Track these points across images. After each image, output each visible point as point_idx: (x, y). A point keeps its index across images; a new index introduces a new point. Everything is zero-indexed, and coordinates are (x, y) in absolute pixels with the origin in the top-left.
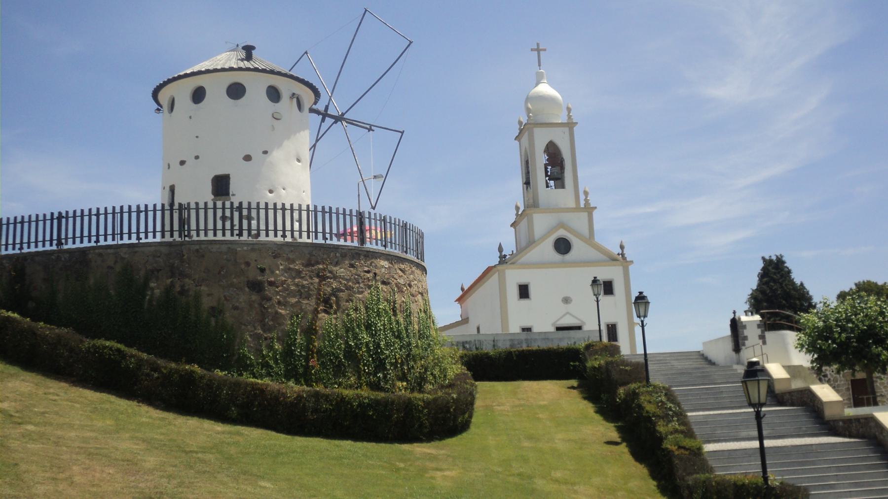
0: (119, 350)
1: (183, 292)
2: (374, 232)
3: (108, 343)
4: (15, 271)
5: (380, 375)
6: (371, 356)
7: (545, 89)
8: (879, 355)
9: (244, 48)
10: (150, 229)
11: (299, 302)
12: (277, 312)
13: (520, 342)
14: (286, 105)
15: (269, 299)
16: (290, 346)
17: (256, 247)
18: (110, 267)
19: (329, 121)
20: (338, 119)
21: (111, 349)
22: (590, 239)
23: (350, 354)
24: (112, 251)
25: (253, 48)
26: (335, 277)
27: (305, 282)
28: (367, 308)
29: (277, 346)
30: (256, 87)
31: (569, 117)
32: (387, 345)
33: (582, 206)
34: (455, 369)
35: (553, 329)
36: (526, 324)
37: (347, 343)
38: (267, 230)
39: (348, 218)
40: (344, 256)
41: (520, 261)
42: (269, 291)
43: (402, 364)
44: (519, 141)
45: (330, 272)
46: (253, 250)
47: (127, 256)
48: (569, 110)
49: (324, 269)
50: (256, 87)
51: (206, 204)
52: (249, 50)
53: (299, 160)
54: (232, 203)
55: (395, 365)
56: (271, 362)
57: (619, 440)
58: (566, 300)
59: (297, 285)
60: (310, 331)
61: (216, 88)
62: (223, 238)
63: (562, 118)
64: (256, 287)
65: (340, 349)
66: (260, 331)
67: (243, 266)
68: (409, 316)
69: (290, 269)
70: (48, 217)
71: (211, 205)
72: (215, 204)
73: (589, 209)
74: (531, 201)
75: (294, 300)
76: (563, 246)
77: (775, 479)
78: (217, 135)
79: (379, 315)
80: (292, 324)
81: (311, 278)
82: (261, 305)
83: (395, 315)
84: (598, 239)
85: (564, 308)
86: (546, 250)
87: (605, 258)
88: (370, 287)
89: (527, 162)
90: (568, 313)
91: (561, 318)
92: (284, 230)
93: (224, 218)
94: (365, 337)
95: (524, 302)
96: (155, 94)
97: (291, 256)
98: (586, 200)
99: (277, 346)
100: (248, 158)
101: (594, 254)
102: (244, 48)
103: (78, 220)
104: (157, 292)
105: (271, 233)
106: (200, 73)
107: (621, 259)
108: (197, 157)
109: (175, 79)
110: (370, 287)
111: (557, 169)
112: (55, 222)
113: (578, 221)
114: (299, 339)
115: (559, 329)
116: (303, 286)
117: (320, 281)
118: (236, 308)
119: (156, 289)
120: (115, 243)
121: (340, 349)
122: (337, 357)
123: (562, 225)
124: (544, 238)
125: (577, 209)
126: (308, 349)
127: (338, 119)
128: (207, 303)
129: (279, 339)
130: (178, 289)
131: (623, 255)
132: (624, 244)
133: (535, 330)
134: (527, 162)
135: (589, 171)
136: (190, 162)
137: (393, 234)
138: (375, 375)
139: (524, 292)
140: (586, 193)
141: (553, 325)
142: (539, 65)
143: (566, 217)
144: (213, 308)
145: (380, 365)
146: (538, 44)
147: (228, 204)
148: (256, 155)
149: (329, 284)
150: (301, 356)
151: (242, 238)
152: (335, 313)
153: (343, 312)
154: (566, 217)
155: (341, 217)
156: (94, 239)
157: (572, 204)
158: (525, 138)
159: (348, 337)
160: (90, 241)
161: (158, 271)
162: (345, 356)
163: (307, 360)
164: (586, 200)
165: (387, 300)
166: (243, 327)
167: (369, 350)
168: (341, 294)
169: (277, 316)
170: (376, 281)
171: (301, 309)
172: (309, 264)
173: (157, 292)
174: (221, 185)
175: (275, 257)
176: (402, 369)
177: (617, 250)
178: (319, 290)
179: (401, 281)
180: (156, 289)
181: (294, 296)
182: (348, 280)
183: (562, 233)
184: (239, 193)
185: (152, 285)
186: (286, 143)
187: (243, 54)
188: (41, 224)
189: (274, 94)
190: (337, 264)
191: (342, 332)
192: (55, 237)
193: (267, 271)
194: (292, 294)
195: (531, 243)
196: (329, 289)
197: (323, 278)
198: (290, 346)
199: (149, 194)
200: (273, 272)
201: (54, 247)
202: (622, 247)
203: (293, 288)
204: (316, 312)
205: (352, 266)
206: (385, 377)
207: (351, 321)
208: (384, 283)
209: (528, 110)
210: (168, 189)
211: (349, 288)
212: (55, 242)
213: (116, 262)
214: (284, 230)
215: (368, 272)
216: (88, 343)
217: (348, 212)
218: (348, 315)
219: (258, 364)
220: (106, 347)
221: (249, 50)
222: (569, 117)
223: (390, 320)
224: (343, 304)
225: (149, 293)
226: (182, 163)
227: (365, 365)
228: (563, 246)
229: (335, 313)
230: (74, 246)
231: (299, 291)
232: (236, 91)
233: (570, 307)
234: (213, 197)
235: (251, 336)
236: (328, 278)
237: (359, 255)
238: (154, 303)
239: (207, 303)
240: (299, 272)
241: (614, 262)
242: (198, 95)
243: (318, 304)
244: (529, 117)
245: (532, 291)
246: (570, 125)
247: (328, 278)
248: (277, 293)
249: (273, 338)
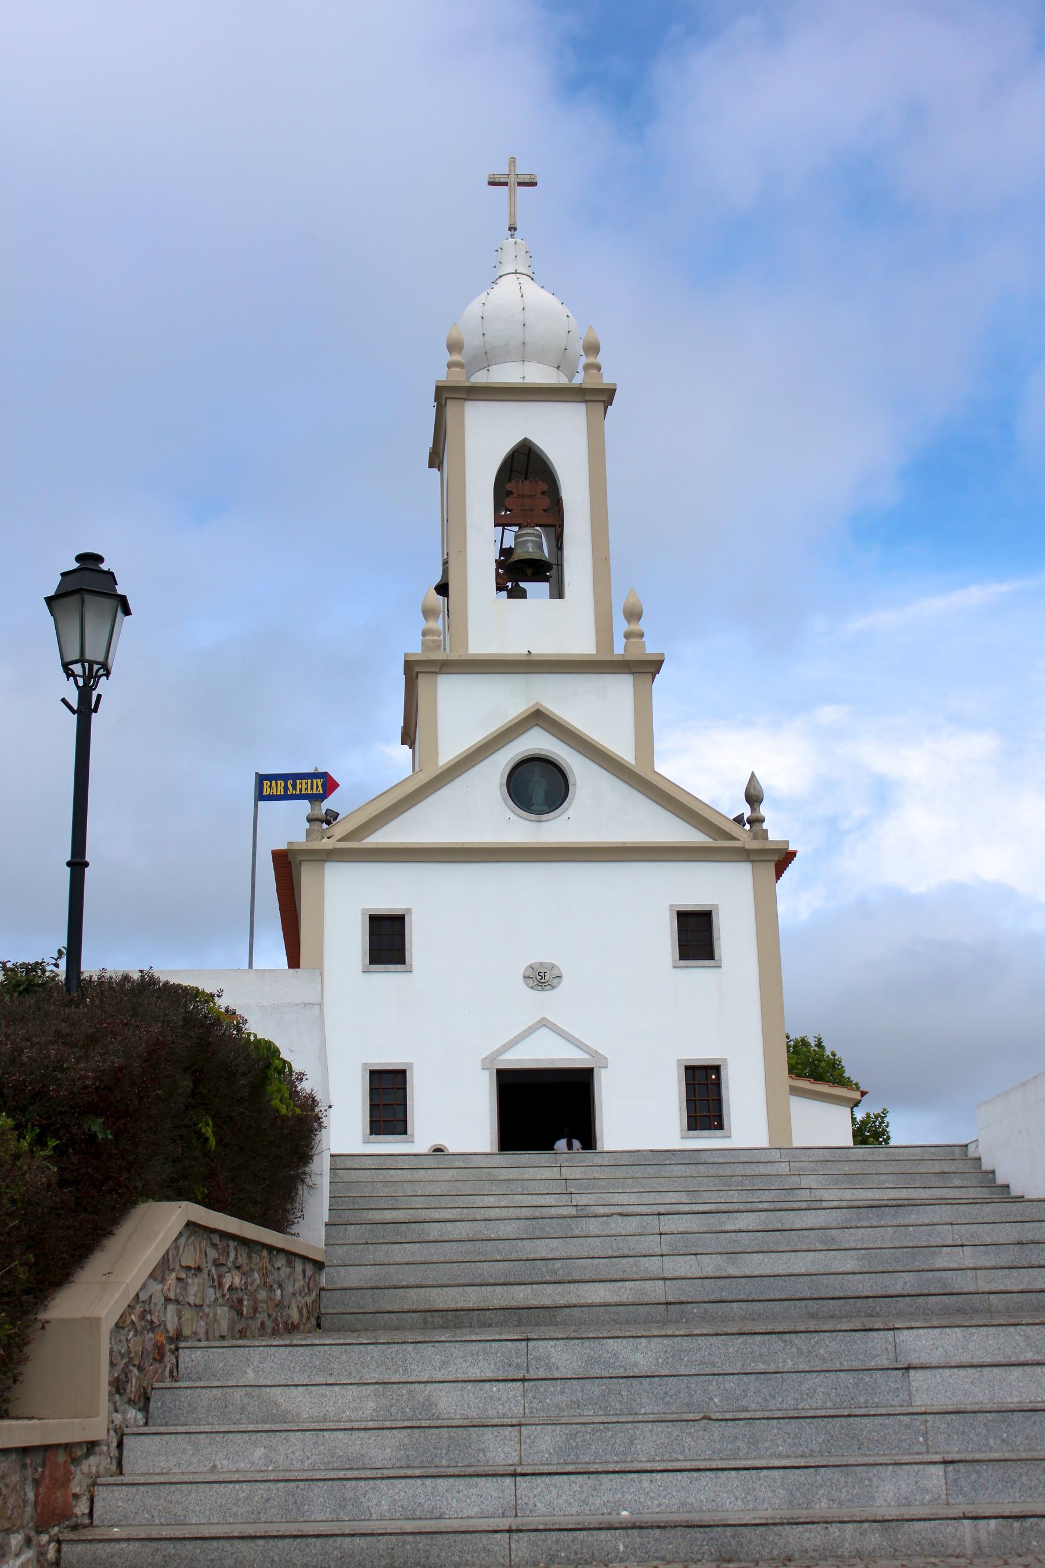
8: (24, 1138)
44: (440, 468)
57: (75, 707)
58: (541, 978)
77: (105, 959)
87: (692, 836)
95: (387, 978)
123: (538, 718)
131: (756, 821)
177: (730, 804)
202: (753, 798)
228: (537, 785)
233: (550, 1004)
245: (418, 939)
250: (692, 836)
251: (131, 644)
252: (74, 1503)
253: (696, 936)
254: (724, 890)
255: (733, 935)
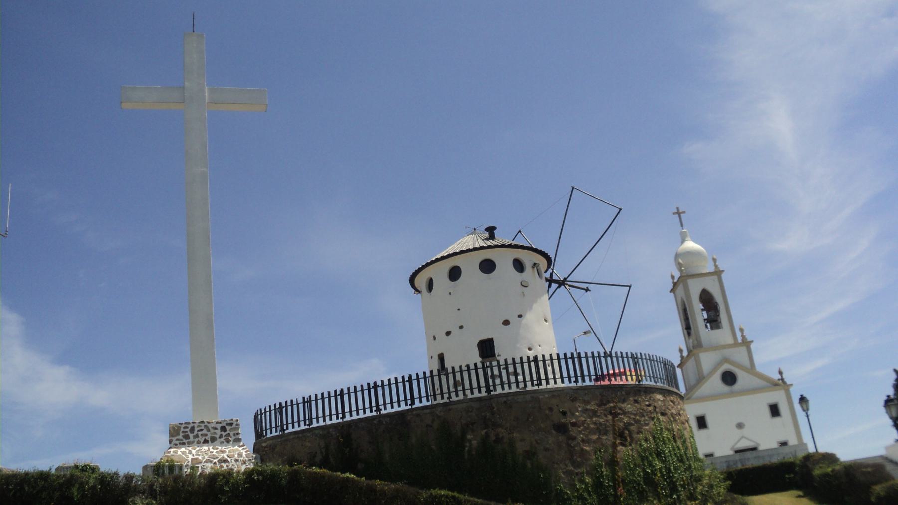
0: (454, 497)
1: (498, 440)
2: (645, 369)
3: (443, 492)
4: (342, 437)
5: (675, 496)
6: (665, 480)
7: (690, 245)
9: (487, 230)
10: (475, 385)
11: (599, 438)
12: (582, 450)
13: (736, 462)
14: (529, 272)
15: (574, 438)
16: (598, 478)
17: (555, 394)
18: (427, 426)
19: (554, 286)
20: (561, 283)
21: (447, 496)
22: (751, 369)
23: (648, 479)
24: (428, 411)
25: (494, 228)
26: (624, 413)
27: (601, 420)
28: (654, 437)
29: (588, 479)
30: (504, 260)
31: (716, 266)
32: (676, 469)
33: (740, 340)
34: (721, 489)
35: (732, 453)
36: (782, 439)
37: (644, 470)
38: (555, 379)
39: (625, 360)
40: (628, 394)
41: (695, 396)
42: (573, 431)
43: (688, 484)
45: (620, 409)
46: (553, 396)
47: (442, 414)
48: (715, 260)
49: (615, 407)
50: (504, 260)
51: (476, 365)
52: (491, 231)
53: (546, 320)
54: (498, 362)
55: (683, 486)
56: (585, 495)
58: (740, 426)
59: (595, 423)
60: (612, 463)
61: (470, 266)
62: (421, 405)
63: (710, 268)
64: (561, 428)
65: (639, 476)
66: (571, 468)
67: (547, 412)
68: (685, 441)
69: (587, 410)
70: (365, 387)
71: (480, 365)
72: (483, 363)
73: (746, 344)
74: (696, 342)
75: (595, 437)
76: (729, 378)
78: (477, 306)
79: (664, 443)
80: (597, 458)
81: (606, 416)
82: (568, 445)
83: (676, 441)
84: (759, 369)
85: (738, 432)
86: (715, 383)
87: (762, 383)
88: (652, 419)
89: (685, 310)
90: (743, 437)
91: (739, 441)
92: (576, 376)
93: (516, 374)
94: (658, 464)
95: (777, 419)
96: (412, 280)
97: (586, 398)
98: (743, 336)
99: (588, 479)
100: (506, 322)
101: (757, 382)
102: (487, 230)
103: (473, 373)
104: (475, 442)
105: (559, 381)
106: (455, 254)
107: (781, 384)
108: (461, 327)
109: (427, 265)
110: (652, 419)
111: (712, 313)
112: (372, 391)
113: (740, 355)
114: (605, 471)
115: (737, 452)
116: (600, 424)
117: (613, 418)
118: (546, 449)
119: (473, 440)
120: (429, 403)
121: (639, 476)
122: (639, 484)
124: (712, 373)
125: (736, 345)
126: (614, 480)
127: (561, 283)
128: (521, 448)
129: (588, 473)
130: (493, 438)
131: (782, 380)
132: (782, 370)
133: (761, 448)
134: (685, 310)
135: (740, 311)
136: (455, 331)
137: (660, 372)
138: (671, 496)
139: (702, 422)
140: (742, 330)
141: (732, 449)
142: (682, 225)
143: (727, 352)
144: (527, 451)
145: (673, 488)
146: (678, 209)
147: (495, 363)
148: (513, 319)
149: (621, 420)
150: (609, 486)
151: (541, 387)
152: (630, 445)
153: (636, 443)
154: (727, 352)
155: (620, 359)
156: (446, 396)
157: (730, 341)
158: (680, 290)
159: (644, 465)
160: (442, 398)
161: (473, 424)
162: (644, 482)
163: (615, 489)
164: (743, 336)
165: (668, 430)
166: (556, 466)
167: (662, 475)
168: (632, 428)
169: (583, 452)
170: (657, 413)
171: (603, 445)
172: (601, 404)
173: (475, 442)
174: (487, 348)
175: (573, 401)
176: (690, 489)
177: (777, 377)
178: (614, 425)
179: (674, 411)
180: (473, 440)
181: (595, 434)
182: (635, 415)
183: (726, 367)
184: (503, 352)
185: (469, 437)
186: (535, 306)
187: (487, 235)
188: (359, 394)
189: (519, 266)
190: (624, 401)
191: (638, 461)
192: (374, 404)
193: (569, 414)
194: (592, 432)
195: (701, 379)
196: (621, 424)
197: (615, 415)
198: (598, 478)
199: (422, 364)
200: (573, 414)
201: (374, 414)
202: (781, 373)
203: (592, 426)
204: (614, 446)
205: (636, 401)
206: (679, 496)
207: (644, 450)
208: (663, 414)
209: (680, 266)
210: (436, 358)
211: (637, 422)
212: (374, 409)
213: (433, 421)
214: (576, 376)
215: (649, 406)
216: (424, 494)
217: (624, 355)
218: (641, 445)
219: (574, 497)
220: (442, 496)
221: (491, 231)
222: (716, 266)
223: (673, 447)
224: (635, 436)
225: (468, 444)
226: (448, 333)
227: (662, 489)
228: (729, 378)
229: (630, 445)
230: (393, 411)
231: (598, 428)
232: (488, 266)
233: (745, 432)
234: (481, 359)
235: (564, 473)
236: (619, 414)
237: (639, 391)
238: (474, 453)
239: (521, 448)
240: (594, 413)
241: (776, 388)
242: (455, 274)
243: (615, 438)
244: (681, 271)
245: (709, 420)
246: (718, 273)
247: (619, 414)
248: (580, 432)
249: (583, 473)
250: (762, 383)
251: (811, 404)
252: (891, 482)
253: (775, 410)
254: (777, 396)
255: (783, 408)
